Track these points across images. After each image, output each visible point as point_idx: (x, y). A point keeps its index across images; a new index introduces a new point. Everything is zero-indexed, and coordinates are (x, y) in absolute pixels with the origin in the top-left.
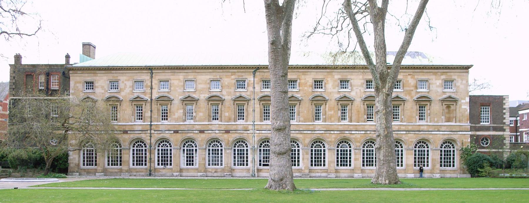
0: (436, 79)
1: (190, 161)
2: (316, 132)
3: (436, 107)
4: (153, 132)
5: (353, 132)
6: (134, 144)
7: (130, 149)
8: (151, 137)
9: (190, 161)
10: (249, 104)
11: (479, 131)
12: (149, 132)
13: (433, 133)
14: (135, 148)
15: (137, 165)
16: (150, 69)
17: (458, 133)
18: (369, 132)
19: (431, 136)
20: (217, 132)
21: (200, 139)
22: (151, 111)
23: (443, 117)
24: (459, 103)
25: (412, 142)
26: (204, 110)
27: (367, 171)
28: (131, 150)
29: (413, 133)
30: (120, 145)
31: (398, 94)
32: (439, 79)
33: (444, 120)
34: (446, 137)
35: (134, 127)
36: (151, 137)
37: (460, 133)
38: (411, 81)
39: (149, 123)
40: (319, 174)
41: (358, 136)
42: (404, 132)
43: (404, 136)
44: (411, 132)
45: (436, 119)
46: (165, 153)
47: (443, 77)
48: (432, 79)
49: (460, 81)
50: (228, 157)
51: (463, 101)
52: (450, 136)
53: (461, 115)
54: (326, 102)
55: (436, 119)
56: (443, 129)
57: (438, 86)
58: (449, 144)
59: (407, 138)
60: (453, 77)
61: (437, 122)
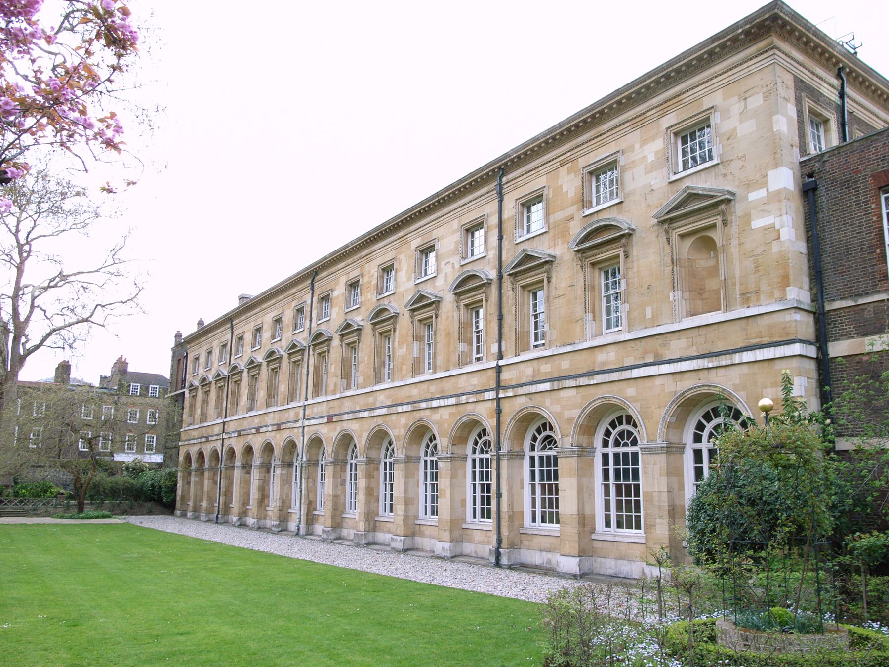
0: (644, 142)
3: (648, 258)
4: (491, 395)
5: (435, 404)
10: (554, 280)
12: (299, 424)
13: (636, 373)
16: (312, 274)
17: (737, 358)
18: (463, 399)
19: (631, 391)
23: (675, 296)
24: (739, 208)
25: (570, 420)
28: (527, 462)
29: (572, 383)
31: (526, 246)
32: (653, 139)
33: (683, 307)
34: (687, 384)
37: (747, 356)
38: (569, 183)
39: (493, 364)
42: (546, 386)
43: (548, 401)
44: (567, 383)
45: (649, 313)
47: (670, 120)
48: (631, 148)
49: (736, 107)
51: (753, 196)
53: (749, 264)
54: (548, 272)
55: (649, 313)
56: (677, 347)
57: (651, 169)
58: (619, 428)
59: (557, 408)
60: (707, 103)
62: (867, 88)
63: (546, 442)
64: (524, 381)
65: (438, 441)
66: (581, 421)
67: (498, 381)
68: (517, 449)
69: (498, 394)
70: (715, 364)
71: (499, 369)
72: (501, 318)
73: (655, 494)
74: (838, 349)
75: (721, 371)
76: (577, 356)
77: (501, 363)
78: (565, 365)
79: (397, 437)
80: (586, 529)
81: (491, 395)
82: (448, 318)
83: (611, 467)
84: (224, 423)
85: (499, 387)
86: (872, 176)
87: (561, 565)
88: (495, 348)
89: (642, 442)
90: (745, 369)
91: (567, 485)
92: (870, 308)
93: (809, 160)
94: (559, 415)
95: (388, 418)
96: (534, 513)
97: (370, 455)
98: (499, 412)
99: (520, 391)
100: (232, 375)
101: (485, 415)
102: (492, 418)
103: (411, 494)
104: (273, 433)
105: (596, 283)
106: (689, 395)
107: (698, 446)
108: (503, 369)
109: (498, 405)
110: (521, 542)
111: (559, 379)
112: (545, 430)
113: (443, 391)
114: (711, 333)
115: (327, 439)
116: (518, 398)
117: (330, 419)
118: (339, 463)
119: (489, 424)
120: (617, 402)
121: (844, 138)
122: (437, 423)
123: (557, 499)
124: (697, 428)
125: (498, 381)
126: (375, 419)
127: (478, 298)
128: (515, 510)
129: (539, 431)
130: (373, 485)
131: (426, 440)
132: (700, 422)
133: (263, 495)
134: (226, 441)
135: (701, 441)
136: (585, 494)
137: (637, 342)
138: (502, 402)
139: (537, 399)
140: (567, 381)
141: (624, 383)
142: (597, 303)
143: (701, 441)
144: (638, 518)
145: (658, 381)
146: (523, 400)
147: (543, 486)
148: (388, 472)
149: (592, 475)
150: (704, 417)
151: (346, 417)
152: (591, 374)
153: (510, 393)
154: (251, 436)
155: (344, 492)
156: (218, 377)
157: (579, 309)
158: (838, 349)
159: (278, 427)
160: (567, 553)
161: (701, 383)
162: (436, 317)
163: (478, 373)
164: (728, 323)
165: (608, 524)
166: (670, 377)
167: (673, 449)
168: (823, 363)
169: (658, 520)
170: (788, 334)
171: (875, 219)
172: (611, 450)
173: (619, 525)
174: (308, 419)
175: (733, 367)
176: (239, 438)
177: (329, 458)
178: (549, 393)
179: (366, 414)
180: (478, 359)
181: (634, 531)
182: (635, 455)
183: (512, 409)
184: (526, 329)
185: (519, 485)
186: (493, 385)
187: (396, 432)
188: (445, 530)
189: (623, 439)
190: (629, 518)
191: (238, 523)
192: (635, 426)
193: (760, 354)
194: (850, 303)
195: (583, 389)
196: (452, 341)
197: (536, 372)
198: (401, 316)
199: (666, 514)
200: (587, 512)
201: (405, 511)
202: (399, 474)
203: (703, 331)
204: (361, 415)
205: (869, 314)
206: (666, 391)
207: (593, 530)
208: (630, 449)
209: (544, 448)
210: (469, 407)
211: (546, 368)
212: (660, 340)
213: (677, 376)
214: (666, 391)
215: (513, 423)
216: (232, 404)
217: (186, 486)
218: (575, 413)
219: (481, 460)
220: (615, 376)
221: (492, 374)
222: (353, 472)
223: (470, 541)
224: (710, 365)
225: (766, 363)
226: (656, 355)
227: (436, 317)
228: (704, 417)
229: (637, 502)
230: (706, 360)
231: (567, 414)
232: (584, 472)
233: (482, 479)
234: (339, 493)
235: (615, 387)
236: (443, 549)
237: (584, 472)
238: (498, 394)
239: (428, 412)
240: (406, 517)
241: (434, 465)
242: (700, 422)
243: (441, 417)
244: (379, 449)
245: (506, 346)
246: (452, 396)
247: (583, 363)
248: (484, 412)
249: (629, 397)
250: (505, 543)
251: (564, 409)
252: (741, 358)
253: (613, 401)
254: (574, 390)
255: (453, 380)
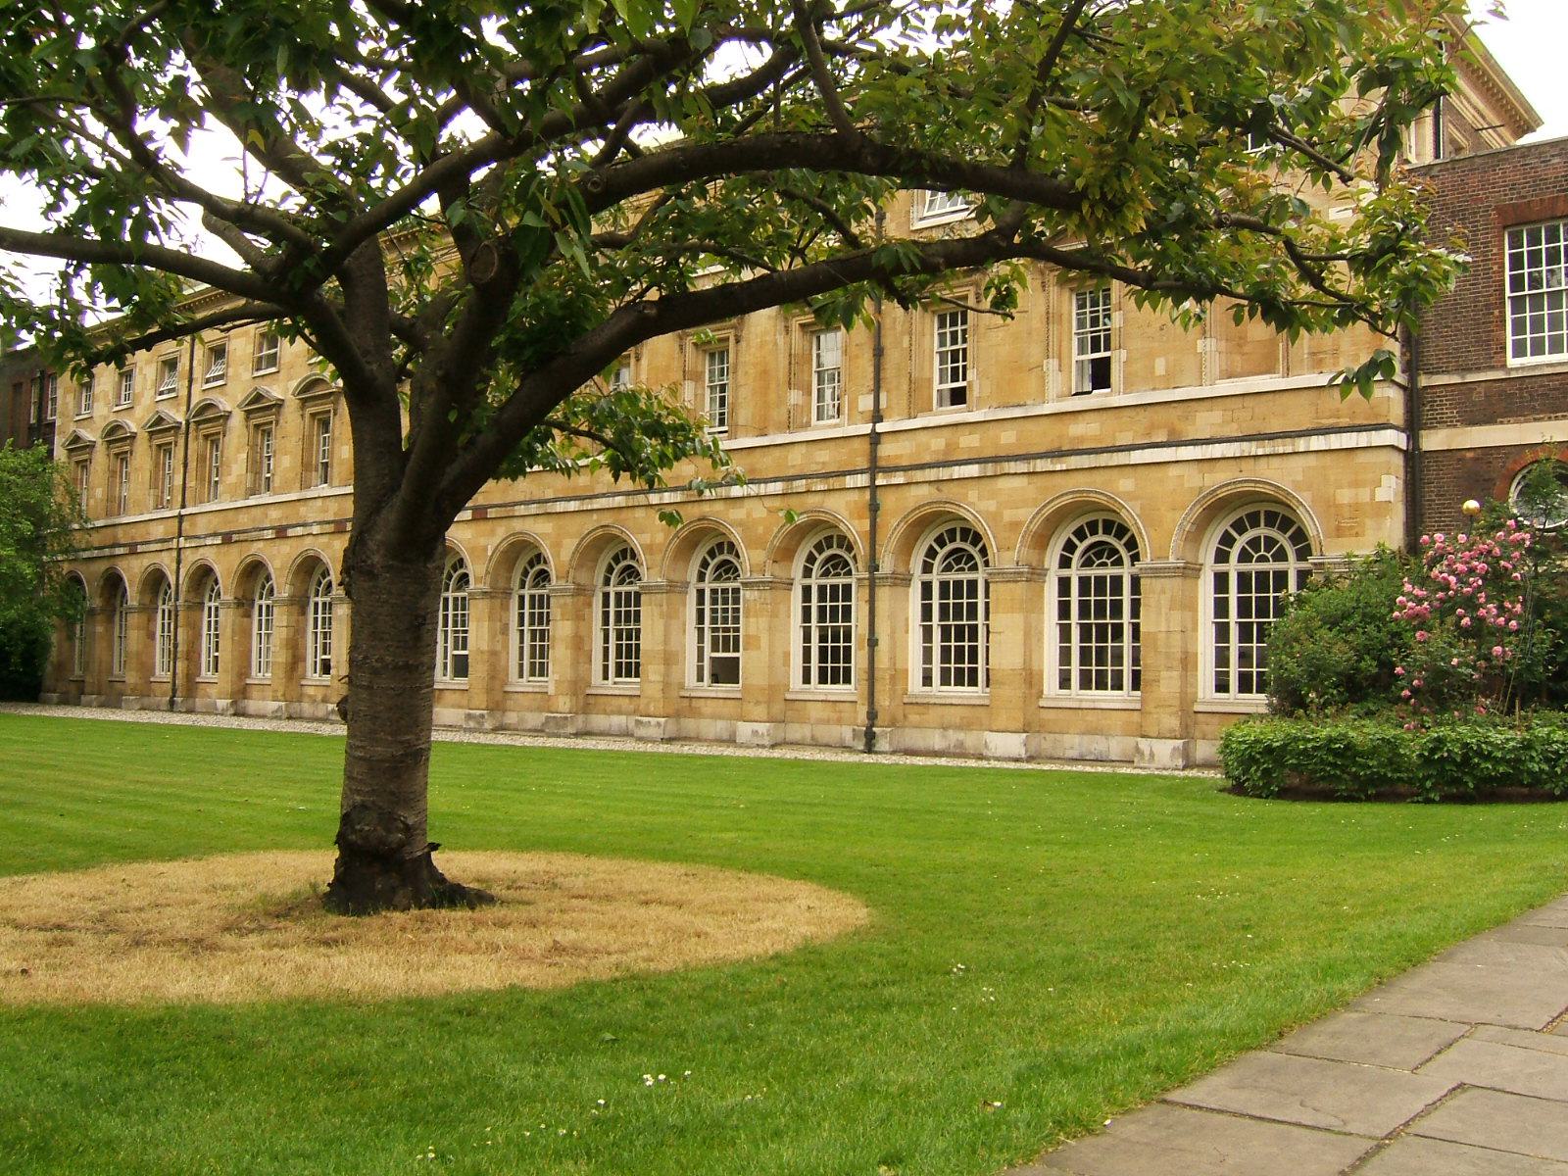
1: (960, 654)
2: (597, 504)
4: (862, 480)
6: (1070, 547)
7: (1037, 574)
8: (179, 562)
9: (960, 654)
11: (1490, 420)
12: (174, 544)
13: (1137, 457)
14: (1233, 568)
15: (1085, 684)
17: (1301, 444)
18: (800, 485)
19: (1125, 484)
20: (316, 529)
21: (278, 563)
22: (186, 466)
25: (1015, 525)
26: (294, 439)
27: (815, 712)
29: (1022, 467)
30: (1299, 536)
33: (1214, 365)
34: (1219, 479)
35: (120, 532)
36: (179, 562)
37: (1317, 443)
39: (867, 429)
40: (954, 736)
41: (759, 511)
42: (973, 470)
43: (972, 493)
45: (1160, 367)
46: (1100, 607)
50: (1026, 632)
52: (1249, 471)
55: (1160, 367)
56: (1206, 422)
58: (1274, 533)
59: (991, 505)
61: (1170, 381)
62: (1484, 83)
63: (950, 559)
64: (927, 459)
65: (273, 581)
66: (1034, 527)
67: (873, 457)
68: (901, 570)
69: (873, 479)
70: (1268, 451)
71: (875, 438)
72: (186, 466)
73: (1162, 636)
74: (1433, 440)
75: (1275, 462)
76: (1029, 425)
77: (880, 428)
78: (1008, 438)
79: (649, 549)
80: (1034, 691)
81: (862, 480)
82: (762, 345)
83: (814, 604)
84: (181, 517)
85: (874, 468)
86: (1496, 208)
87: (991, 745)
88: (866, 403)
89: (745, 575)
90: (1311, 460)
91: (561, 629)
92: (1481, 389)
93: (1410, 171)
94: (994, 518)
95: (625, 514)
96: (521, 666)
97: (578, 580)
98: (874, 508)
99: (919, 475)
100: (198, 423)
101: (846, 514)
102: (860, 517)
103: (674, 646)
104: (324, 539)
105: (1065, 311)
106: (1222, 493)
107: (1065, 572)
108: (884, 439)
109: (873, 497)
110: (905, 716)
111: (996, 460)
112: (625, 558)
113: (752, 471)
114: (1261, 406)
115: (472, 551)
116: (913, 487)
117: (227, 539)
118: (244, 604)
119: (855, 528)
120: (1103, 500)
121: (1437, 156)
122: (740, 524)
123: (638, 646)
124: (807, 561)
125: (873, 457)
126: (595, 516)
127: (326, 407)
128: (898, 666)
129: (712, 554)
130: (583, 632)
131: (317, 576)
132: (931, 547)
133: (294, 656)
134: (185, 554)
135: (1069, 567)
136: (579, 644)
137: (1141, 410)
138: (878, 492)
139: (949, 492)
140: (1012, 464)
141: (1116, 471)
142: (1065, 344)
143: (1069, 567)
144: (847, 671)
145: (1173, 471)
146: (925, 490)
147: (533, 632)
148: (264, 618)
149: (1041, 611)
150: (815, 547)
151: (521, 510)
152: (1059, 454)
153: (899, 478)
154: (261, 544)
155: (506, 646)
156: (158, 426)
157: (1035, 351)
158: (1433, 440)
159: (281, 533)
160: (1002, 728)
161: (943, 497)
162: (738, 341)
163: (833, 443)
164: (1292, 395)
165: (700, 678)
166: (1195, 466)
167: (581, 591)
168: (1413, 459)
169: (1164, 674)
170: (1377, 416)
171: (1495, 268)
172: (527, 592)
173: (823, 680)
174: (187, 538)
175: (1296, 457)
176: (225, 548)
177: (228, 597)
178: (974, 482)
179: (573, 506)
180: (958, 397)
181: (966, 688)
182: (847, 588)
183: (903, 503)
184: (927, 375)
185: (901, 629)
186: (862, 463)
187: (646, 538)
188: (758, 703)
189: (1267, 550)
190: (835, 670)
191: (232, 711)
192: (737, 556)
193: (1336, 441)
194: (1455, 379)
195: (1040, 477)
196: (773, 386)
197: (950, 446)
198: (287, 404)
199: (1176, 663)
200: (1035, 668)
201: (667, 675)
202: (478, 611)
203: (1249, 402)
204: (560, 507)
205: (1478, 396)
206: (1186, 485)
207: (505, 683)
208: (840, 581)
209: (948, 568)
210: (812, 501)
211: (969, 442)
212: (1179, 410)
213: (1206, 465)
214: (1186, 485)
215: (903, 527)
216: (200, 479)
217: (66, 645)
218: (1025, 514)
219: (456, 599)
220: (1104, 459)
221: (864, 446)
222: (213, 619)
223: (803, 720)
224: (1260, 452)
225: (1343, 454)
226: (1172, 431)
227: (738, 341)
228: (815, 547)
229: (848, 650)
230: (1254, 443)
231: (1008, 515)
232: (580, 617)
233: (532, 623)
234: (499, 647)
235: (1098, 478)
236: (755, 733)
237: (580, 617)
238: (873, 479)
239: (719, 506)
240: (666, 686)
241: (541, 602)
242: (931, 547)
243: (749, 515)
244: (593, 569)
245: (888, 400)
246: (775, 480)
247: (1042, 437)
248: (845, 509)
249: (1125, 494)
250: (882, 718)
251: (1004, 508)
252: (855, 482)
253: (1093, 498)
254: (1024, 480)
255: (777, 452)
